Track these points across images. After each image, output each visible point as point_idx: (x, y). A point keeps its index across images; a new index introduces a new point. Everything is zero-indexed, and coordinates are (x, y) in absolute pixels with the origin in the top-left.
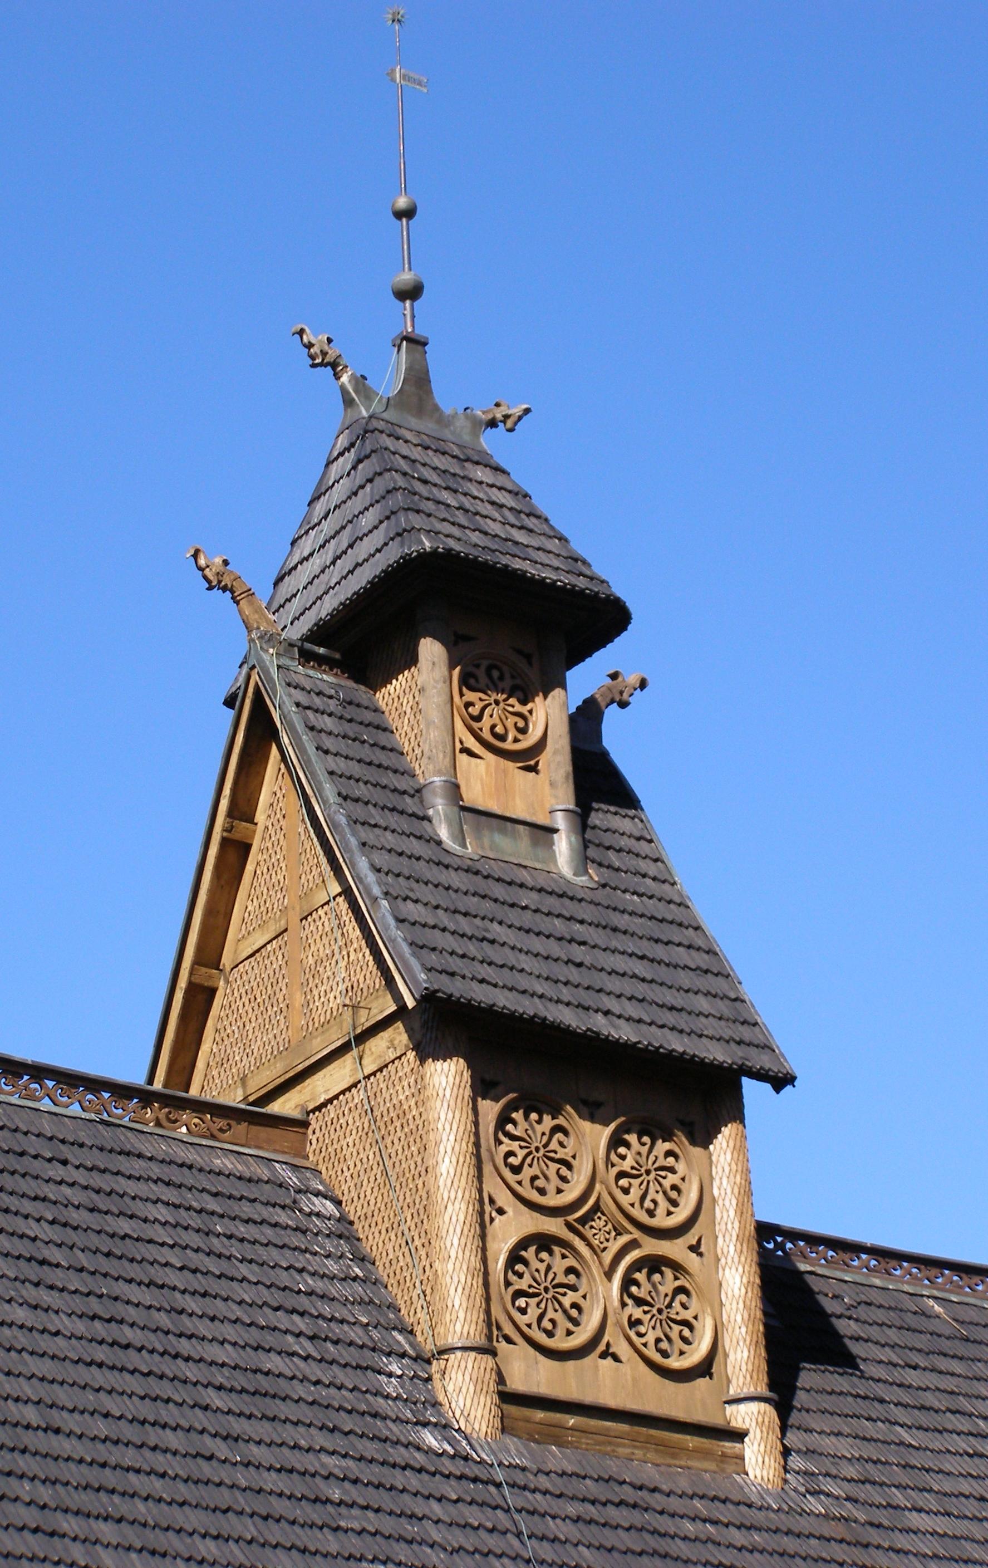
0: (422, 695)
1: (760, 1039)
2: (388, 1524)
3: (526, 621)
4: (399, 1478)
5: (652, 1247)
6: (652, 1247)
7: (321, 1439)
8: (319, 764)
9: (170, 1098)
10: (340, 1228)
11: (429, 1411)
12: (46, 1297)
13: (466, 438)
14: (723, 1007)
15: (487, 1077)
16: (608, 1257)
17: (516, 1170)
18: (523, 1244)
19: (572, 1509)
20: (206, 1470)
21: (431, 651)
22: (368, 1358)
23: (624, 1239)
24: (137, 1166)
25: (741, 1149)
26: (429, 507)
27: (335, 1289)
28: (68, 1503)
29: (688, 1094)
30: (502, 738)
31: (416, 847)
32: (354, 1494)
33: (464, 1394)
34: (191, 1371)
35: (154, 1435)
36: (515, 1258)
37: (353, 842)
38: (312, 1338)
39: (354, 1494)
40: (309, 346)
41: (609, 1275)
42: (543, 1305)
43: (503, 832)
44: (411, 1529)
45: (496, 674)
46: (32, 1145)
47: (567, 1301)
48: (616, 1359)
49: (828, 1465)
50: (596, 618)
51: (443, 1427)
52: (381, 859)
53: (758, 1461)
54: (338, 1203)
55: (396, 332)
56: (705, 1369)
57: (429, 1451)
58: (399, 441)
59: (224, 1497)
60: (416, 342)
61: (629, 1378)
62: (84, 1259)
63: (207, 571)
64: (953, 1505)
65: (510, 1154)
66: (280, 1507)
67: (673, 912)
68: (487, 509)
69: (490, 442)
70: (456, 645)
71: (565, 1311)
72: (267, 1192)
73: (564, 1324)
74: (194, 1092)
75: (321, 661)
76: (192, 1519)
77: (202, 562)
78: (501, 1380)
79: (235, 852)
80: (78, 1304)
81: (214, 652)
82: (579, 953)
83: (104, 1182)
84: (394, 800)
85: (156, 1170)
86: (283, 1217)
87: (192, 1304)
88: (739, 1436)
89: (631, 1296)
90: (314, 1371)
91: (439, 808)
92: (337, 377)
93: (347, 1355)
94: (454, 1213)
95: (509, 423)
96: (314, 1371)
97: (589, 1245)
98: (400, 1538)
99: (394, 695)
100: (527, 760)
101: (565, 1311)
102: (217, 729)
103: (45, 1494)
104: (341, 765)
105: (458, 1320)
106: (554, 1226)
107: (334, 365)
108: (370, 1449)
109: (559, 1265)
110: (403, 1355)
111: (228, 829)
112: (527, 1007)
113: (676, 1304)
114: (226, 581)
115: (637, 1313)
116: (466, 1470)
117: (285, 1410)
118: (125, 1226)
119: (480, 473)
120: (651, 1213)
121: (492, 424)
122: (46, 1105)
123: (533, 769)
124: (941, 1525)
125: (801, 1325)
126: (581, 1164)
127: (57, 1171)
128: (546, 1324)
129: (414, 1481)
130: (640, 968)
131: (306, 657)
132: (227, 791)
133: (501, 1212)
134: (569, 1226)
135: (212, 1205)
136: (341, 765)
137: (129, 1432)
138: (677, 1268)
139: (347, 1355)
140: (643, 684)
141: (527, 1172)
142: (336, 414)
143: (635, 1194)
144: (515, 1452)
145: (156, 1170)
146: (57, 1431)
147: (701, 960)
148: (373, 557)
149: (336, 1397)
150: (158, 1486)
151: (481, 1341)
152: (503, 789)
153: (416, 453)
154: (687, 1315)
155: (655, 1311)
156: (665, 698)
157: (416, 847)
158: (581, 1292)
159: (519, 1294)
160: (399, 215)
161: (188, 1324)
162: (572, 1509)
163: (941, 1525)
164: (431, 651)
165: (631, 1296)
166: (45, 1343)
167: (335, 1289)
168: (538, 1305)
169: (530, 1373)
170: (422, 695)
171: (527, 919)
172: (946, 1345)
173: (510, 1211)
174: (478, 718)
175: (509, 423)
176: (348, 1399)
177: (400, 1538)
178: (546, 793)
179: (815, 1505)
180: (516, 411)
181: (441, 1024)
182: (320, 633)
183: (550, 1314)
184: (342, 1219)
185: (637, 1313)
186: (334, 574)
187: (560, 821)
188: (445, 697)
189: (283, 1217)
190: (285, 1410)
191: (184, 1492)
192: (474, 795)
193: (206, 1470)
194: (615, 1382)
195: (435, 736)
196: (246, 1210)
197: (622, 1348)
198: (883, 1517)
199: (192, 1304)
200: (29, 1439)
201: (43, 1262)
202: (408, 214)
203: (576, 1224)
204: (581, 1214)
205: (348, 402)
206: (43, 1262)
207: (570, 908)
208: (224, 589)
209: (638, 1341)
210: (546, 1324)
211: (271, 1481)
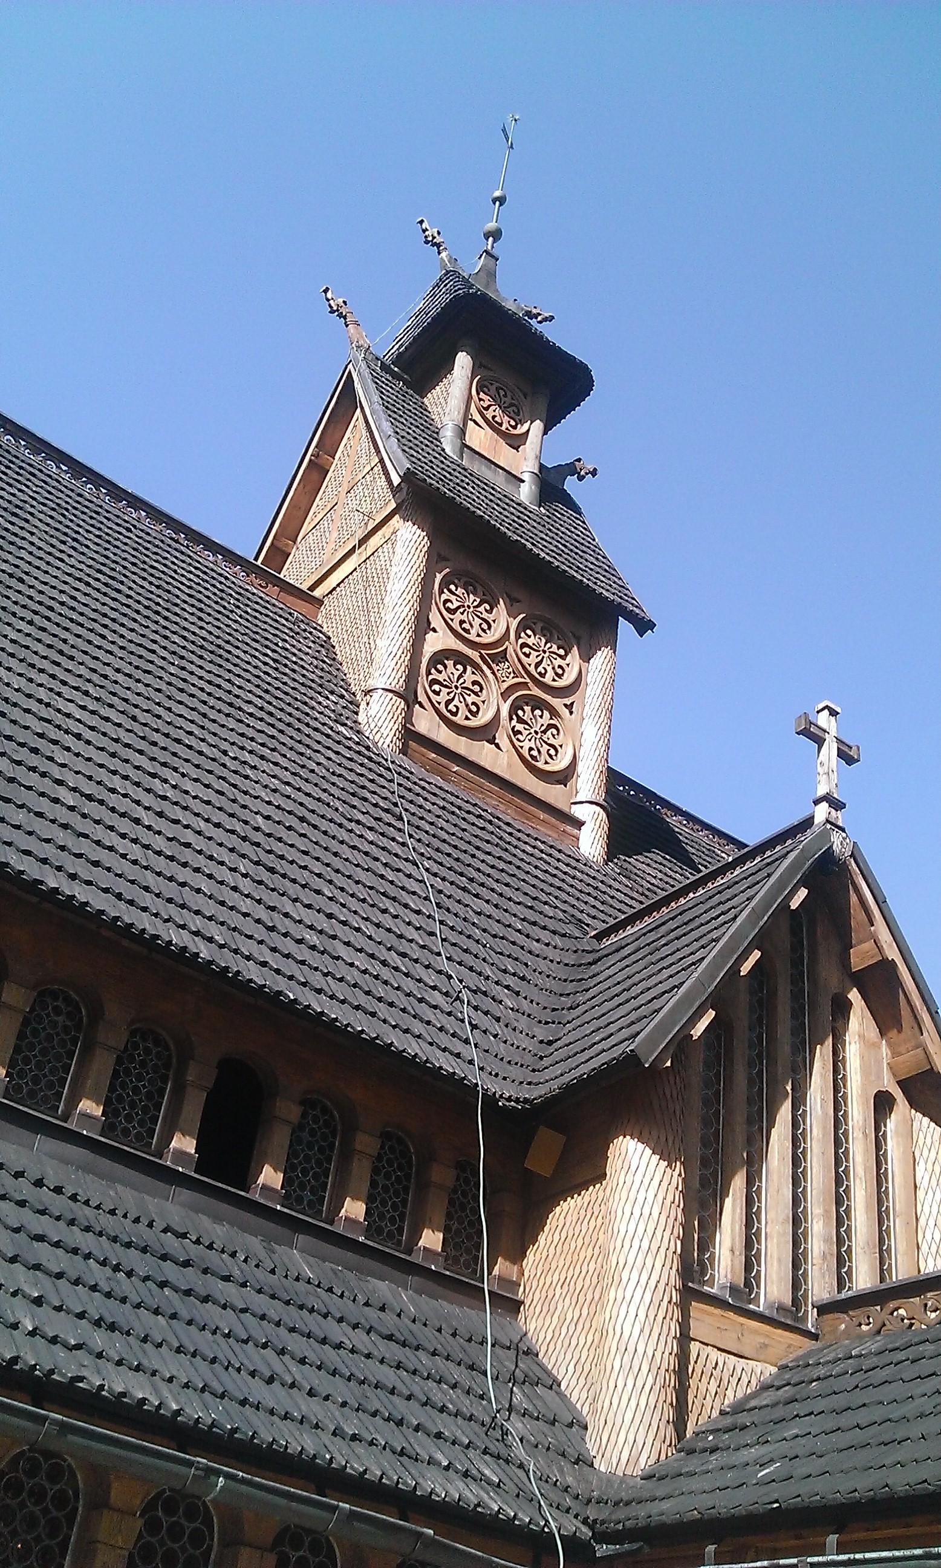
15: (443, 553)
16: (505, 685)
21: (463, 361)
29: (581, 610)
42: (452, 695)
45: (502, 393)
47: (469, 700)
48: (498, 746)
56: (564, 777)
61: (505, 762)
63: (331, 302)
71: (467, 705)
77: (329, 295)
88: (579, 824)
89: (517, 716)
92: (439, 253)
97: (493, 673)
101: (467, 705)
102: (320, 398)
107: (438, 245)
109: (469, 677)
111: (316, 455)
113: (549, 733)
114: (344, 311)
115: (519, 727)
116: (365, 749)
120: (543, 675)
123: (517, 449)
126: (498, 625)
128: (451, 707)
133: (434, 630)
134: (482, 657)
138: (554, 713)
140: (594, 473)
141: (458, 616)
155: (532, 731)
158: (482, 699)
159: (435, 682)
160: (494, 201)
165: (517, 716)
168: (448, 694)
173: (441, 633)
182: (399, 359)
183: (456, 702)
185: (519, 727)
188: (466, 393)
194: (497, 758)
197: (502, 739)
202: (501, 200)
204: (496, 655)
208: (340, 315)
209: (517, 743)
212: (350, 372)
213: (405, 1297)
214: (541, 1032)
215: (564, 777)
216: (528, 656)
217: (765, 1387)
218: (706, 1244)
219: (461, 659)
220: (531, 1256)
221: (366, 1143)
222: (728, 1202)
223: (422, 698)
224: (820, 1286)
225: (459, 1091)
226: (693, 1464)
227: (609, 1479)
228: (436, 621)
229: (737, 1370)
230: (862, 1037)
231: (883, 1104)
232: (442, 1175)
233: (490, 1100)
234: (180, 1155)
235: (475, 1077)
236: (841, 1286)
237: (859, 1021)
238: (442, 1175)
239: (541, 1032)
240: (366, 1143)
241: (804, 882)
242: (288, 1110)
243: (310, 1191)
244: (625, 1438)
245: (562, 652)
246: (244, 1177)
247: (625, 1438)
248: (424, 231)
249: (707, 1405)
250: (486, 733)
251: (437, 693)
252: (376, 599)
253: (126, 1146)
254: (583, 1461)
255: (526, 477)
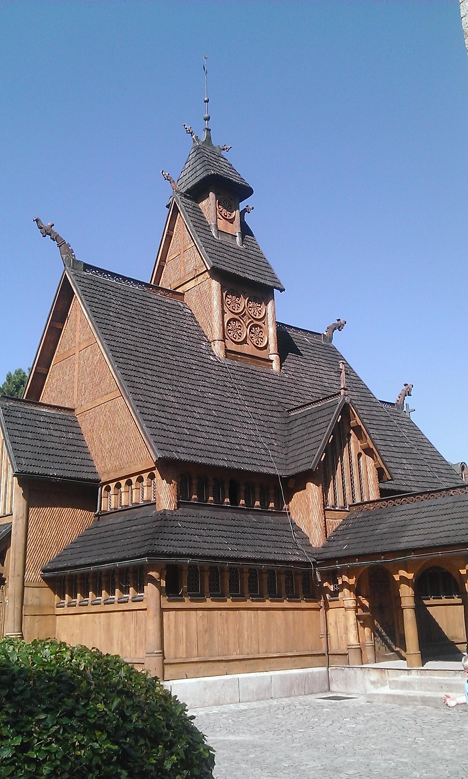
0: (209, 205)
1: (278, 282)
2: (205, 374)
3: (232, 192)
4: (206, 365)
5: (256, 322)
6: (256, 322)
7: (191, 357)
8: (189, 219)
9: (156, 288)
10: (192, 315)
11: (211, 352)
12: (134, 325)
13: (218, 152)
14: (270, 275)
17: (229, 305)
18: (230, 320)
19: (240, 373)
20: (168, 361)
21: (212, 195)
22: (199, 341)
23: (250, 320)
24: (151, 300)
25: (274, 304)
26: (212, 165)
27: (191, 327)
28: (141, 366)
30: (226, 216)
31: (208, 237)
32: (197, 367)
33: (218, 349)
34: (164, 341)
35: (158, 354)
36: (229, 322)
37: (197, 235)
38: (187, 337)
39: (197, 367)
40: (186, 128)
41: (247, 328)
43: (226, 236)
44: (209, 375)
46: (129, 294)
49: (288, 368)
50: (245, 192)
51: (214, 356)
52: (203, 239)
53: (275, 366)
54: (191, 310)
55: (204, 127)
56: (266, 347)
57: (212, 360)
58: (205, 151)
59: (172, 367)
60: (208, 130)
62: (141, 318)
64: (312, 378)
65: (228, 301)
66: (183, 369)
67: (259, 255)
68: (224, 167)
69: (223, 153)
70: (217, 195)
72: (177, 307)
73: (238, 337)
74: (160, 286)
75: (188, 198)
76: (165, 370)
78: (226, 347)
79: (169, 237)
80: (140, 326)
81: (166, 194)
82: (242, 261)
83: (144, 303)
84: (204, 227)
85: (155, 301)
86: (180, 312)
87: (163, 328)
88: (272, 361)
90: (189, 343)
91: (213, 230)
93: (194, 340)
94: (217, 313)
95: (228, 150)
96: (189, 343)
98: (207, 377)
99: (203, 205)
100: (231, 221)
102: (166, 213)
103: (136, 364)
104: (193, 219)
105: (217, 335)
106: (237, 317)
108: (200, 359)
110: (206, 341)
112: (234, 271)
117: (183, 350)
118: (149, 312)
119: (222, 159)
120: (255, 316)
121: (224, 150)
122: (131, 286)
124: (310, 381)
125: (287, 342)
127: (134, 300)
128: (234, 336)
129: (209, 366)
130: (254, 266)
131: (185, 196)
132: (168, 224)
135: (166, 309)
136: (193, 219)
137: (152, 352)
138: (261, 327)
139: (194, 340)
142: (192, 144)
143: (252, 311)
144: (228, 362)
145: (155, 301)
146: (138, 351)
147: (266, 265)
148: (201, 175)
149: (193, 348)
150: (159, 364)
151: (222, 339)
152: (226, 227)
153: (209, 154)
154: (262, 336)
156: (259, 210)
157: (208, 237)
160: (205, 102)
161: (163, 332)
162: (240, 373)
163: (310, 381)
164: (212, 195)
166: (134, 334)
167: (191, 327)
169: (232, 346)
170: (209, 205)
171: (232, 254)
172: (308, 347)
174: (221, 212)
175: (228, 150)
176: (195, 349)
177: (207, 377)
178: (235, 229)
179: (286, 375)
180: (229, 147)
181: (216, 273)
182: (188, 191)
184: (192, 314)
185: (252, 335)
186: (191, 179)
187: (237, 234)
189: (180, 312)
190: (183, 350)
191: (164, 365)
192: (220, 227)
193: (168, 361)
194: (247, 349)
195: (213, 214)
196: (173, 311)
197: (249, 342)
198: (299, 379)
199: (163, 328)
200: (132, 352)
201: (133, 318)
202: (207, 101)
203: (272, 330)
204: (242, 315)
205: (194, 142)
206: (133, 318)
207: (239, 252)
210: (234, 336)
211: (181, 364)
212: (175, 202)
213: (270, 518)
214: (284, 451)
215: (266, 347)
216: (251, 311)
217: (341, 525)
218: (327, 495)
219: (234, 320)
220: (290, 503)
221: (257, 490)
222: (330, 489)
223: (227, 337)
224: (349, 501)
225: (275, 476)
226: (330, 544)
227: (315, 548)
228: (226, 310)
229: (335, 522)
230: (354, 441)
231: (359, 455)
232: (272, 492)
233: (281, 476)
234: (228, 503)
235: (278, 473)
236: (353, 502)
237: (353, 438)
238: (272, 492)
239: (284, 451)
240: (257, 490)
241: (340, 415)
242: (243, 488)
243: (249, 503)
244: (317, 540)
245: (260, 305)
246: (238, 504)
247: (317, 540)
248: (186, 128)
249: (331, 529)
250: (244, 342)
251: (230, 334)
252: (207, 302)
253: (219, 506)
254: (310, 545)
255: (237, 234)
